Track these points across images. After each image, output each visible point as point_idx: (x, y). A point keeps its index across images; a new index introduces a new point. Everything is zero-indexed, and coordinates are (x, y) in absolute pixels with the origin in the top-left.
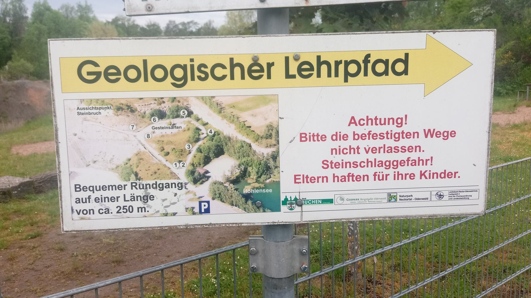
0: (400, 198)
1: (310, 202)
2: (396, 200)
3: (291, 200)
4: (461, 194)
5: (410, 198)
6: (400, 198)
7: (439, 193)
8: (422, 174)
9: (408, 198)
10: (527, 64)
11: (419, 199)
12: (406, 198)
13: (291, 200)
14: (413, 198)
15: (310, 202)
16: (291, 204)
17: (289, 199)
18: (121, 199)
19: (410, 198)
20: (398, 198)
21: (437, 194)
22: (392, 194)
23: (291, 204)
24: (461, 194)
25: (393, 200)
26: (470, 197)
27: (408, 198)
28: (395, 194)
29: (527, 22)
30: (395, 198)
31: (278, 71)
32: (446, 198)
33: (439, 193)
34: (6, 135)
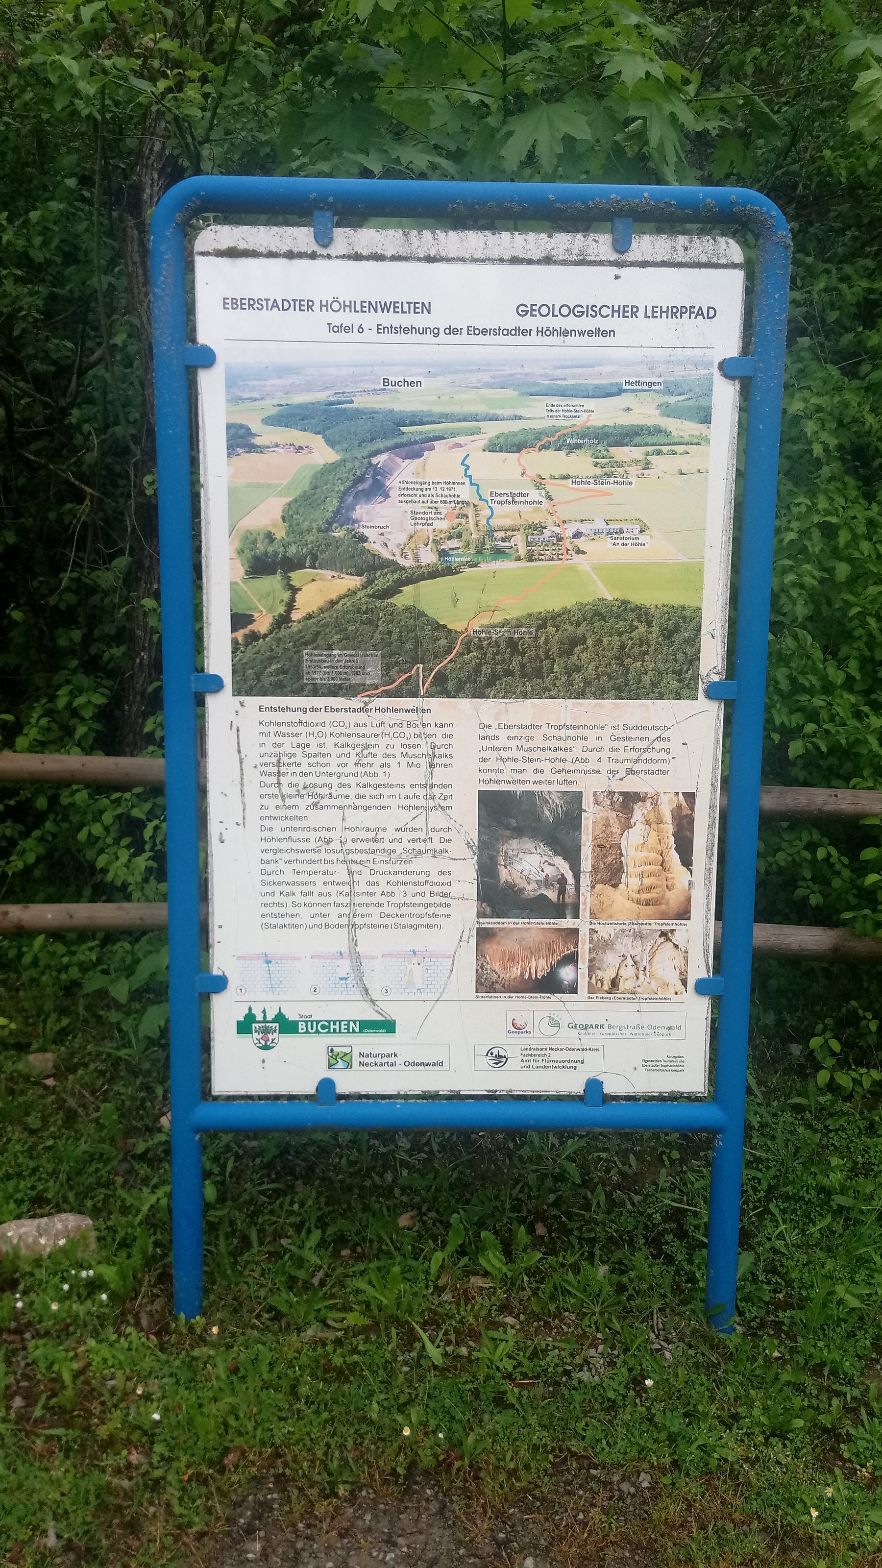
1: (323, 1027)
2: (349, 1065)
4: (556, 1055)
5: (391, 1060)
7: (495, 1051)
9: (385, 1060)
14: (399, 1060)
15: (323, 1027)
17: (259, 1017)
19: (391, 1060)
21: (489, 1052)
22: (336, 1049)
23: (266, 1031)
24: (556, 1055)
25: (341, 1064)
26: (578, 1065)
27: (385, 1060)
28: (348, 1050)
29: (877, 463)
30: (347, 1058)
31: (534, 333)
32: (513, 1064)
33: (495, 1051)
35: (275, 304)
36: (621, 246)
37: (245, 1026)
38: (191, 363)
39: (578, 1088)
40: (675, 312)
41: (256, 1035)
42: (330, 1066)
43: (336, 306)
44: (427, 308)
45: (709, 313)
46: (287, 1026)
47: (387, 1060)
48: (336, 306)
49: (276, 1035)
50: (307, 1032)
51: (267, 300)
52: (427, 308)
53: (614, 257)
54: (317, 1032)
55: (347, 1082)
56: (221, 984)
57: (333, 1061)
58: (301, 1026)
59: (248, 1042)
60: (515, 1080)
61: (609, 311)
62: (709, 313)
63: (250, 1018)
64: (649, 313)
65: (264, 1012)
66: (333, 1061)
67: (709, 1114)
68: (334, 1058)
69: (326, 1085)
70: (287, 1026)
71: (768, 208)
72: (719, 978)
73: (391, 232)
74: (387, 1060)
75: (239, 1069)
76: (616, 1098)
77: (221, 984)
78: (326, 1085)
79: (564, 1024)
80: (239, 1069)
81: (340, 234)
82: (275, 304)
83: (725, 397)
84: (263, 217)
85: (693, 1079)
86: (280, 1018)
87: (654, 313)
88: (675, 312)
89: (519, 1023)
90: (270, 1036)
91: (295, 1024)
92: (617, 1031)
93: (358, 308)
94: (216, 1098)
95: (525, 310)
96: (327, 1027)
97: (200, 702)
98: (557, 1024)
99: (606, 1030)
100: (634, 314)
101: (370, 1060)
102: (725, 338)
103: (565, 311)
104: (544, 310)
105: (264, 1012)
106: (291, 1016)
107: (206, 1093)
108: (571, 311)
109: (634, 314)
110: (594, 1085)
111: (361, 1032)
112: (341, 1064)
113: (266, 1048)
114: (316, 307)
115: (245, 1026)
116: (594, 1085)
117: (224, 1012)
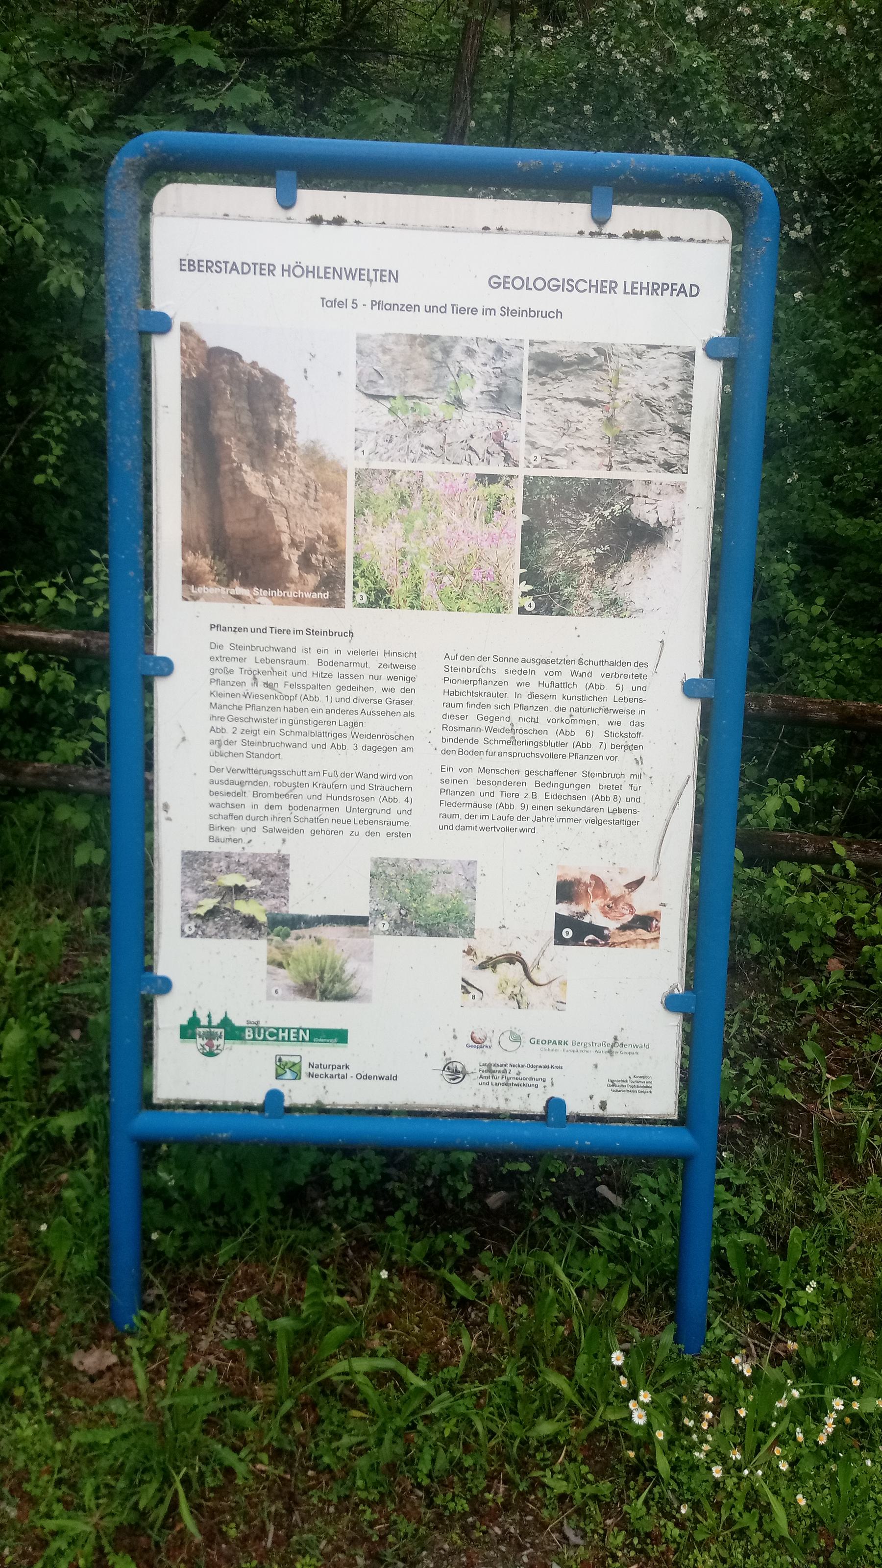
0: (311, 1070)
3: (210, 1026)
5: (342, 1072)
6: (311, 1070)
8: (615, 797)
9: (335, 1072)
10: (4, 1350)
11: (370, 1078)
12: (329, 1072)
13: (210, 1026)
14: (351, 1072)
16: (211, 1037)
17: (204, 1021)
18: (570, 745)
19: (342, 1072)
20: (305, 1069)
22: (284, 1059)
23: (211, 1037)
25: (289, 1075)
27: (335, 1072)
28: (296, 1060)
30: (295, 1069)
34: (224, 413)
35: (234, 267)
36: (600, 218)
37: (188, 1031)
38: (144, 327)
39: (537, 1107)
40: (656, 289)
41: (200, 1041)
42: (278, 1076)
43: (298, 271)
44: (394, 276)
45: (689, 291)
46: (233, 1032)
47: (339, 1071)
48: (298, 271)
49: (221, 1041)
50: (254, 1039)
51: (226, 263)
52: (394, 276)
53: (595, 228)
54: (265, 1039)
55: (299, 1093)
56: (166, 986)
57: (280, 1071)
58: (248, 1034)
59: (192, 1047)
60: (466, 1096)
61: (587, 286)
62: (689, 291)
63: (194, 1021)
64: (629, 289)
65: (209, 1016)
66: (280, 1071)
67: (682, 1139)
68: (283, 1068)
69: (274, 1096)
70: (233, 1032)
71: (758, 182)
72: (690, 994)
73: (705, 212)
74: (339, 1071)
75: (182, 1074)
76: (302, 1109)
77: (166, 986)
78: (274, 1096)
79: (526, 1040)
80: (182, 1074)
81: (618, 211)
82: (234, 267)
83: (709, 378)
84: (445, 188)
85: (662, 1101)
86: (226, 1023)
87: (635, 288)
88: (656, 289)
89: (477, 1036)
90: (215, 1042)
91: (242, 1029)
92: (581, 1048)
93: (322, 274)
94: (160, 1107)
95: (499, 283)
96: (274, 1035)
97: (149, 688)
98: (517, 1039)
99: (570, 1047)
100: (612, 289)
101: (318, 1071)
102: (706, 316)
103: (540, 284)
104: (518, 283)
105: (209, 1016)
106: (238, 1022)
107: (146, 1100)
108: (547, 284)
109: (612, 289)
110: (555, 1105)
111: (311, 1041)
112: (289, 1075)
113: (211, 1054)
114: (620, 289)
115: (188, 1031)
116: (555, 1105)
117: (169, 1014)
